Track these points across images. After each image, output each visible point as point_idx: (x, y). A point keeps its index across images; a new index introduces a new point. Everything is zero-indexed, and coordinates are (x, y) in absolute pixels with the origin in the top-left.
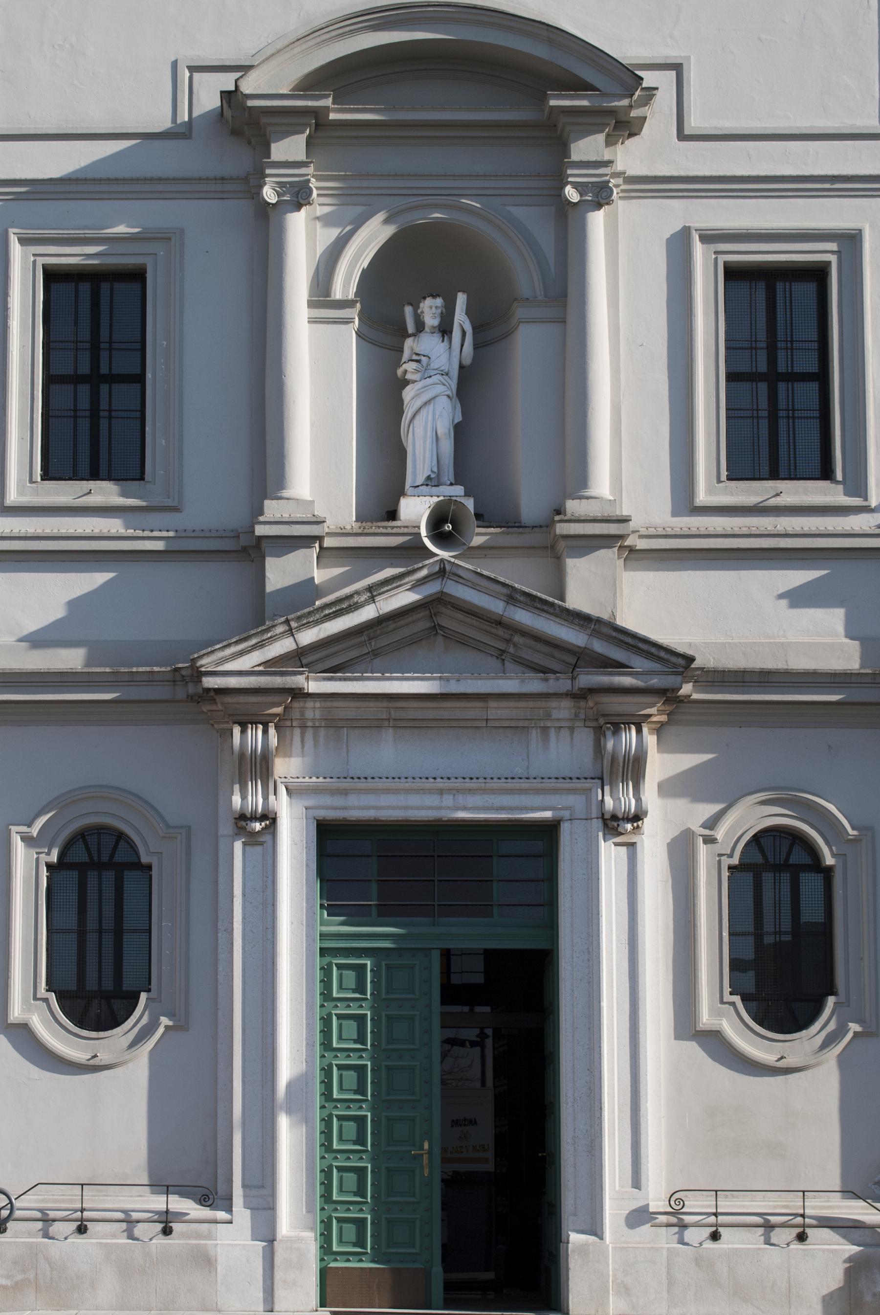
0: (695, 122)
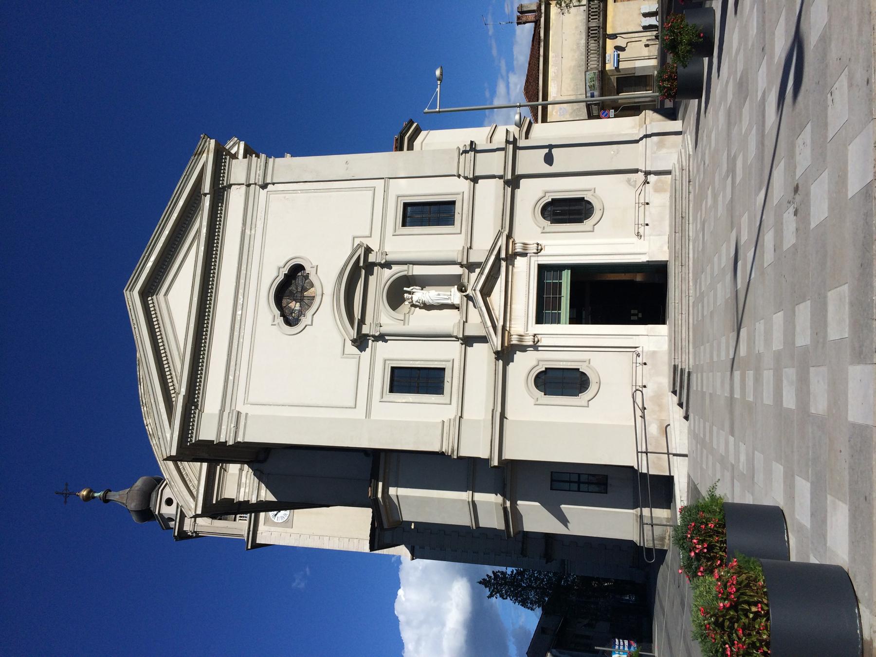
0: (368, 234)
